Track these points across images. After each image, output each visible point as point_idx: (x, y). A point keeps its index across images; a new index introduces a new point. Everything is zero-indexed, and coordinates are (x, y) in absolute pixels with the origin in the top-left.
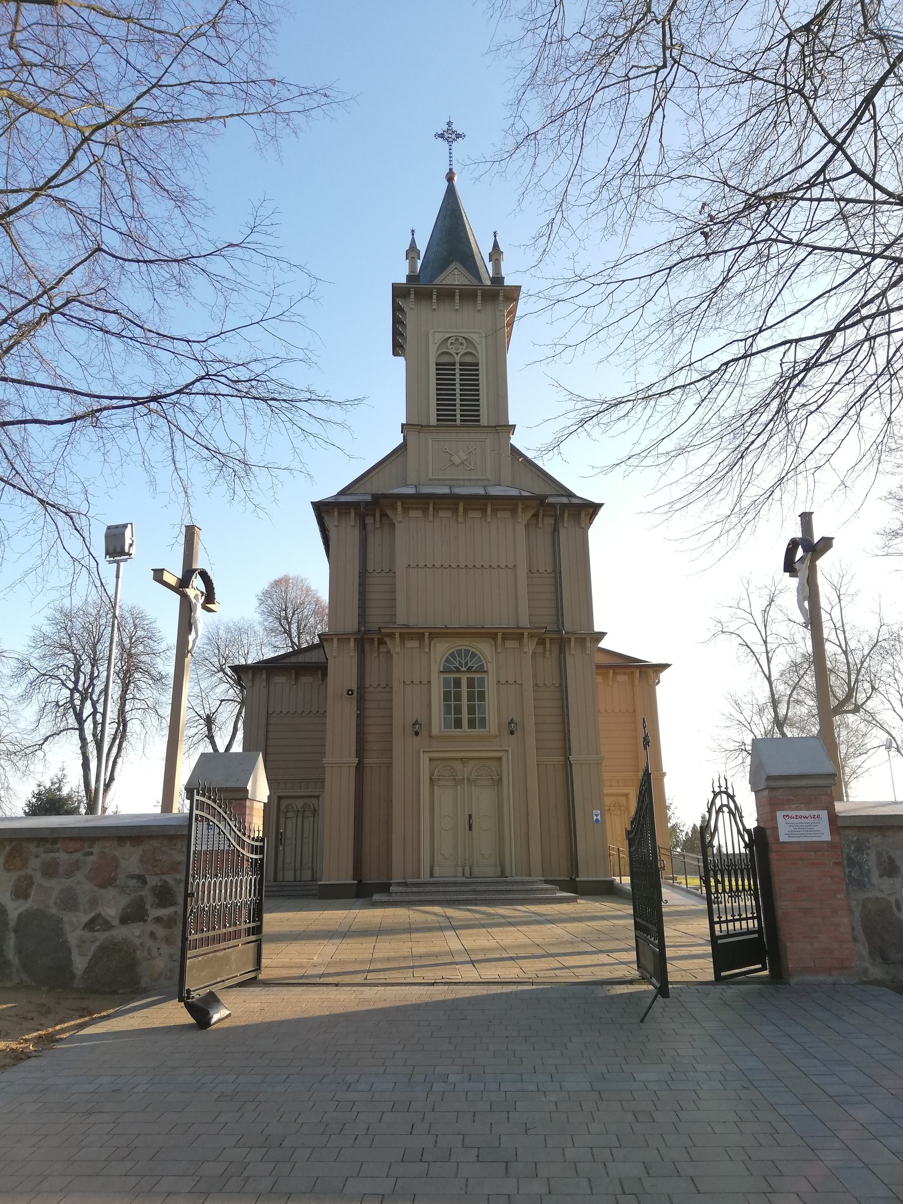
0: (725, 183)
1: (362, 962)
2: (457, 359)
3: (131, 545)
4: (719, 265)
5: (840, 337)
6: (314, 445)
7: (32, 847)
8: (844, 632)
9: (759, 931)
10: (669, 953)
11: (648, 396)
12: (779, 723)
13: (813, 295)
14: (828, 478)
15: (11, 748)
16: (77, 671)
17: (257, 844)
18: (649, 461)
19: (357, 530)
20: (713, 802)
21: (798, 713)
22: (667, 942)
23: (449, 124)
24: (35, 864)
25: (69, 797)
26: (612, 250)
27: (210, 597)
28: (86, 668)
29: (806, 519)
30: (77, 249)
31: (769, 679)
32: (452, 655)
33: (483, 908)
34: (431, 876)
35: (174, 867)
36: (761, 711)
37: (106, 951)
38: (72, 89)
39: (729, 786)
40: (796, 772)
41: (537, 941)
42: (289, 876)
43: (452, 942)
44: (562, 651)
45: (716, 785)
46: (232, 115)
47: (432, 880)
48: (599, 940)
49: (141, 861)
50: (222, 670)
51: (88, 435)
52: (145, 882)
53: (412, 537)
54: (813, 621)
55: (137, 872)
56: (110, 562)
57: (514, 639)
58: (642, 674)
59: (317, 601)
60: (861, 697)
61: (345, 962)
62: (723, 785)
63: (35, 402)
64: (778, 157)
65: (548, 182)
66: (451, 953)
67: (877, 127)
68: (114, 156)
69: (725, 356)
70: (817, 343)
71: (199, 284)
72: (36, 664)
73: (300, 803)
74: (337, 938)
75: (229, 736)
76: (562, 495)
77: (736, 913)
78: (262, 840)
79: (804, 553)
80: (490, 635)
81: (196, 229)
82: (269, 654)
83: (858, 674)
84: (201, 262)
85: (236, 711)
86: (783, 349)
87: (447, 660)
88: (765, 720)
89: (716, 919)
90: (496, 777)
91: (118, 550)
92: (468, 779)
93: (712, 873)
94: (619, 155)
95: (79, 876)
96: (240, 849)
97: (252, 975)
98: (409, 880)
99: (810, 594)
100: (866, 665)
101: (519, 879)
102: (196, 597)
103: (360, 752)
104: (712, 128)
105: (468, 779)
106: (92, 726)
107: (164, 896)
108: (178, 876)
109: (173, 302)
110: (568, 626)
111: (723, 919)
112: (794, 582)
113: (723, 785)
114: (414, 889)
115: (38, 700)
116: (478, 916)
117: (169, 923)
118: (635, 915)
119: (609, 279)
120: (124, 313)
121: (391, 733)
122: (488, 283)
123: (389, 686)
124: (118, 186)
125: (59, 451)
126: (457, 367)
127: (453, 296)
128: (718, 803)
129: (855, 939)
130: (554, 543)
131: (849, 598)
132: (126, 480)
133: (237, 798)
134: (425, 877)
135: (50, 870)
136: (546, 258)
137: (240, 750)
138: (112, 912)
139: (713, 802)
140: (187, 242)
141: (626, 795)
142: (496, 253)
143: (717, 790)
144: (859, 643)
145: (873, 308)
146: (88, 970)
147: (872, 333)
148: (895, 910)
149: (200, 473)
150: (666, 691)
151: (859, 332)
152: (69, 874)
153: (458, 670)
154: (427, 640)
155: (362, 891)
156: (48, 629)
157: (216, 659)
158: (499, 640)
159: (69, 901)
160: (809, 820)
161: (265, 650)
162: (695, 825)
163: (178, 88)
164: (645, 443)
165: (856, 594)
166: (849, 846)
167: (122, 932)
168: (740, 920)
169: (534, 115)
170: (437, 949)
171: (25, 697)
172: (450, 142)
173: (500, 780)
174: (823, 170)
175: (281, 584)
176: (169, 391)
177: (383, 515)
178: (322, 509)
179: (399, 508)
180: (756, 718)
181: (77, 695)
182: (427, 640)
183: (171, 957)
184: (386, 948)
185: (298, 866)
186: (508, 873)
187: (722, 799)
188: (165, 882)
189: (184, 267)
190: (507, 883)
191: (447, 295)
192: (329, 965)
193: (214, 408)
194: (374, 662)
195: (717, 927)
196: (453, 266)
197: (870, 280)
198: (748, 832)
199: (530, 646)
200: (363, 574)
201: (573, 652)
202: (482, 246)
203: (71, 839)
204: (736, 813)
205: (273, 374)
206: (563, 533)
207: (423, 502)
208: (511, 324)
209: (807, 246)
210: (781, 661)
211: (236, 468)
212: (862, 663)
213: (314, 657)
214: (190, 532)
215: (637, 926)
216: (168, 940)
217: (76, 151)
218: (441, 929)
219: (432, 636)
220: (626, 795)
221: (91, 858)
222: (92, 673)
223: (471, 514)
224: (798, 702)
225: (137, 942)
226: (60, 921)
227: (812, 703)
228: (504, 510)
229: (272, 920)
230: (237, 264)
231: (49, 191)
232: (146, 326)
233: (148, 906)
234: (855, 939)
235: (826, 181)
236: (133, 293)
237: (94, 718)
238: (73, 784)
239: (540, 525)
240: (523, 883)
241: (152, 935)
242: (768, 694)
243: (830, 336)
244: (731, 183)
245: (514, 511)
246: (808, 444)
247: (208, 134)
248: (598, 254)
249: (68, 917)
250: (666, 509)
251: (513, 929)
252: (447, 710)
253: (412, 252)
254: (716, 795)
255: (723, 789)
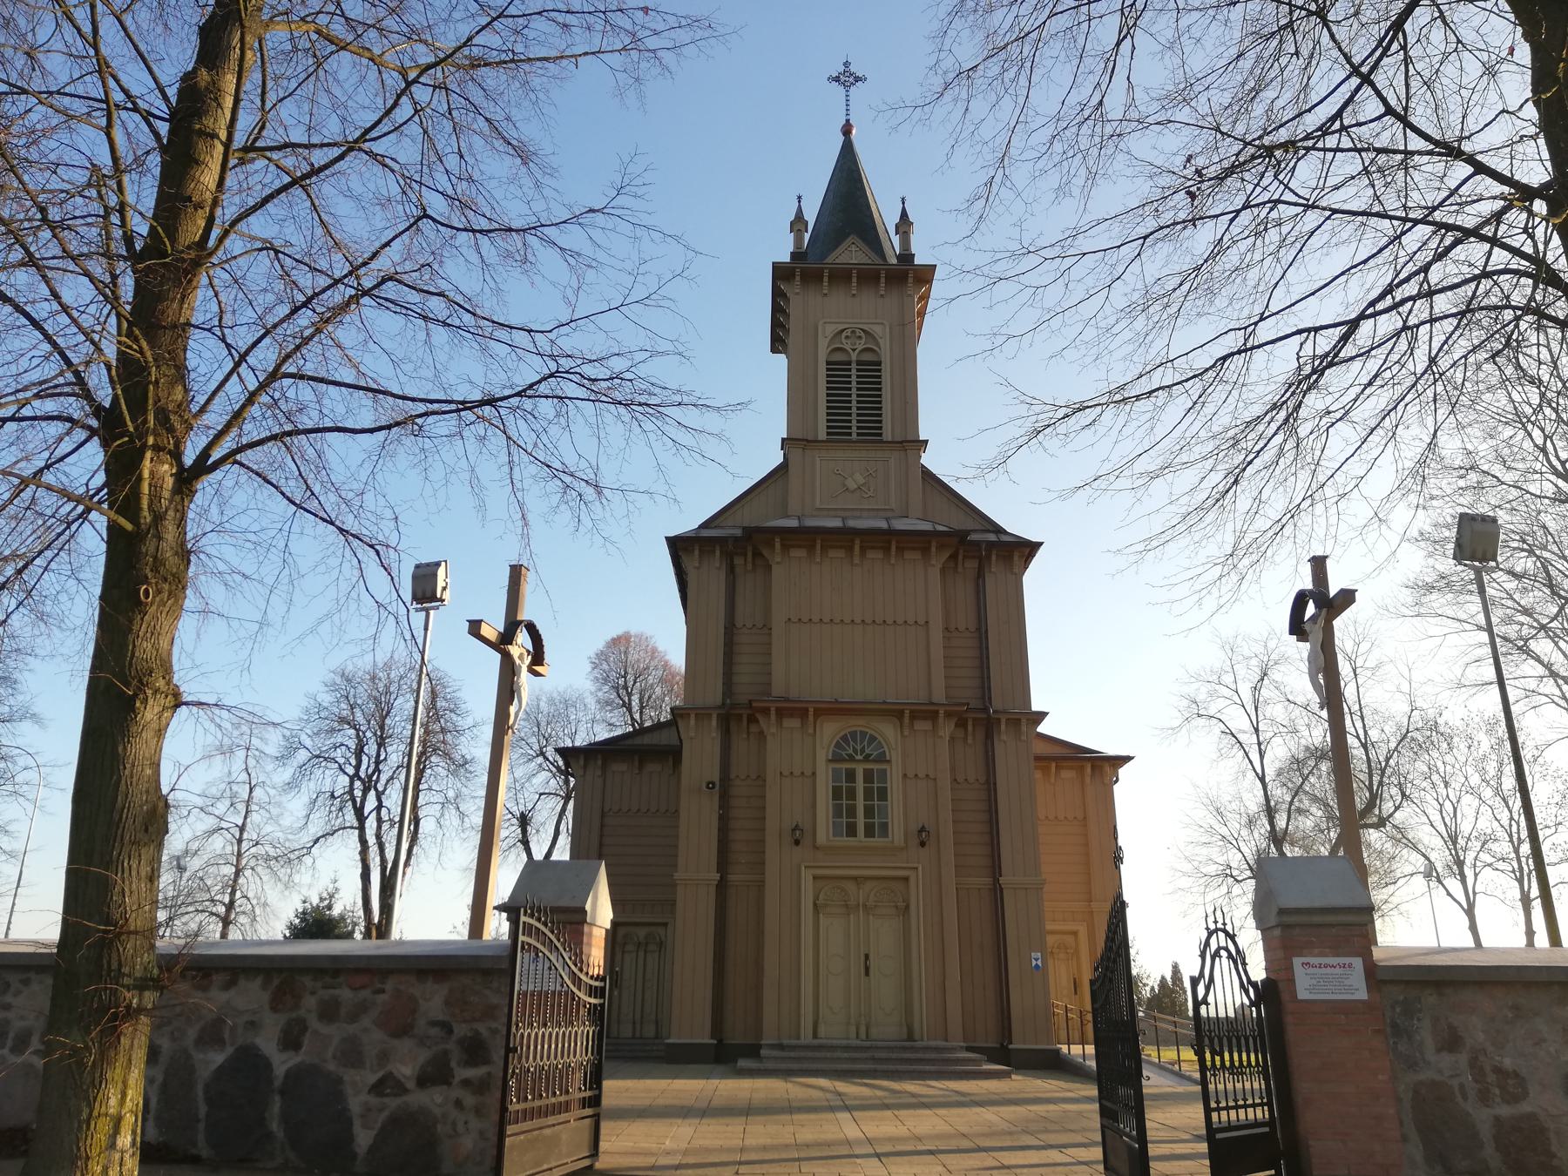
0: (1217, 129)
1: (730, 1150)
2: (854, 357)
3: (444, 589)
4: (1205, 235)
5: (1366, 327)
6: (689, 460)
7: (307, 981)
8: (1362, 718)
9: (1271, 1123)
10: (1153, 1150)
11: (1120, 398)
12: (1277, 838)
13: (1332, 271)
14: (1356, 509)
15: (272, 852)
16: (359, 752)
17: (597, 984)
18: (1123, 483)
19: (723, 576)
20: (1207, 944)
21: (1301, 826)
22: (1150, 1135)
23: (847, 64)
24: (310, 1002)
25: (342, 918)
26: (1066, 215)
27: (538, 657)
28: (371, 749)
29: (1319, 565)
30: (402, 213)
31: (1262, 779)
32: (844, 738)
33: (885, 1083)
34: (815, 1036)
35: (489, 1012)
36: (1251, 823)
37: (402, 1122)
38: (390, 23)
39: (1228, 921)
40: (1317, 904)
41: (963, 1129)
42: (627, 1031)
43: (848, 1127)
44: (989, 736)
45: (1211, 919)
46: (586, 54)
47: (816, 1042)
48: (1047, 1131)
49: (447, 1003)
50: (542, 754)
51: (406, 446)
52: (451, 1031)
53: (796, 583)
54: (1332, 697)
55: (441, 1018)
56: (417, 610)
57: (925, 719)
58: (1100, 769)
59: (666, 666)
60: (1388, 807)
61: (708, 1150)
62: (1220, 921)
63: (337, 405)
64: (1279, 97)
65: (986, 132)
66: (848, 1142)
67: (1407, 61)
68: (440, 102)
69: (1219, 350)
70: (1337, 332)
71: (546, 258)
72: (308, 742)
73: (642, 933)
74: (695, 1116)
75: (553, 841)
76: (989, 531)
77: (1240, 1097)
78: (603, 979)
79: (1317, 610)
80: (895, 713)
81: (547, 192)
82: (603, 734)
83: (1382, 775)
84: (551, 232)
85: (559, 808)
86: (1298, 339)
87: (838, 745)
88: (1256, 835)
89: (1213, 1105)
90: (901, 904)
91: (428, 594)
92: (865, 906)
93: (1207, 1041)
94: (1073, 100)
95: (366, 1021)
96: (575, 990)
97: (587, 1163)
98: (785, 1042)
99: (1326, 668)
100: (1392, 762)
101: (933, 1043)
102: (521, 657)
103: (723, 864)
104: (1197, 63)
105: (865, 906)
106: (375, 825)
107: (475, 1051)
108: (494, 1025)
109: (513, 281)
110: (997, 703)
111: (1223, 1104)
112: (1305, 647)
113: (1220, 921)
114: (792, 1054)
115: (309, 789)
116: (879, 1093)
117: (480, 1087)
118: (1101, 1098)
119: (1066, 249)
120: (451, 295)
121: (763, 841)
122: (894, 261)
123: (761, 778)
124: (446, 142)
125: (368, 467)
126: (854, 366)
127: (850, 278)
128: (1214, 946)
129: (1405, 1139)
130: (978, 593)
131: (1369, 673)
132: (450, 507)
133: (573, 921)
134: (806, 1037)
135: (329, 1012)
136: (982, 226)
137: (566, 857)
138: (406, 1071)
139: (1207, 944)
140: (538, 206)
141: (1075, 933)
142: (904, 224)
143: (1212, 927)
144: (1382, 733)
145: (1411, 289)
146: (372, 1150)
147: (1412, 321)
148: (1459, 1099)
149: (540, 495)
150: (1127, 791)
151: (1388, 323)
152: (353, 1018)
153: (851, 759)
154: (811, 718)
155: (725, 1052)
156: (326, 699)
157: (534, 740)
158: (906, 720)
159: (352, 1054)
160: (1338, 970)
161: (597, 728)
162: (1163, 978)
163: (521, 20)
164: (1116, 460)
165: (1378, 667)
166: (1393, 1008)
167: (419, 1099)
168: (1245, 1106)
169: (967, 49)
170: (829, 1136)
171: (292, 785)
172: (847, 86)
173: (907, 907)
174: (1339, 115)
175: (620, 643)
176: (507, 392)
177: (757, 554)
178: (678, 546)
179: (778, 545)
180: (1245, 832)
181: (358, 784)
182: (811, 718)
183: (481, 1133)
184: (761, 1133)
185: (638, 1016)
186: (917, 1035)
187: (1218, 943)
188: (477, 1033)
189: (531, 239)
190: (913, 1049)
191: (841, 276)
192: (686, 1153)
193: (558, 415)
194: (742, 746)
195: (1215, 1115)
196: (850, 240)
197: (1402, 253)
198: (1254, 985)
199: (947, 729)
200: (730, 629)
201: (1004, 737)
202: (887, 216)
203: (358, 971)
204: (1238, 959)
205: (642, 370)
206: (990, 581)
207: (807, 539)
208: (922, 314)
209: (1324, 209)
210: (1278, 753)
211: (582, 491)
212: (1387, 760)
213: (665, 738)
214: (516, 573)
215: (1104, 1112)
216: (478, 1111)
217: (399, 96)
218: (832, 1109)
219: (818, 713)
220: (1075, 933)
221: (381, 998)
222: (378, 755)
223: (871, 554)
224: (1300, 811)
225: (437, 1111)
226: (340, 1081)
227: (1320, 813)
228: (914, 549)
229: (615, 1089)
230: (596, 234)
231: (366, 146)
232: (479, 312)
233: (453, 1064)
234: (1405, 1139)
235: (1343, 128)
236: (461, 271)
237: (379, 813)
238: (347, 901)
239: (960, 569)
240: (937, 1049)
241: (458, 1104)
242: (1262, 800)
243: (1353, 325)
244: (1224, 129)
245: (925, 551)
246: (1328, 465)
247: (554, 77)
248: (1051, 223)
249: (349, 1075)
250: (1141, 547)
251: (927, 1112)
252: (838, 812)
253: (798, 222)
254: (1210, 934)
255: (1220, 925)
